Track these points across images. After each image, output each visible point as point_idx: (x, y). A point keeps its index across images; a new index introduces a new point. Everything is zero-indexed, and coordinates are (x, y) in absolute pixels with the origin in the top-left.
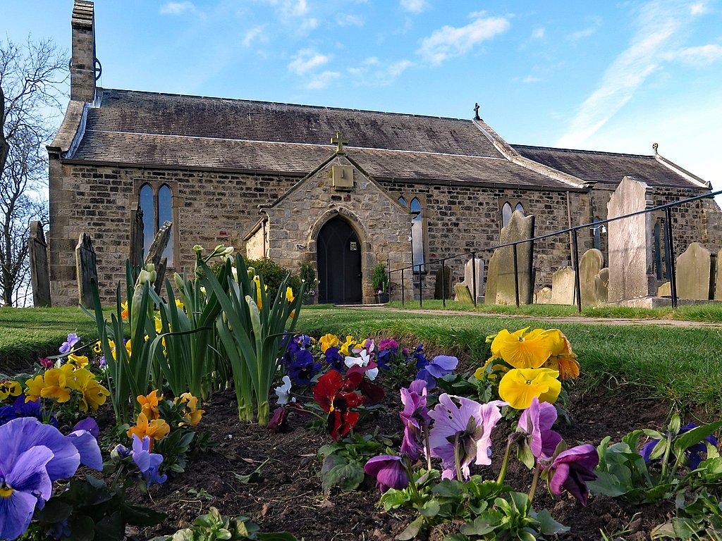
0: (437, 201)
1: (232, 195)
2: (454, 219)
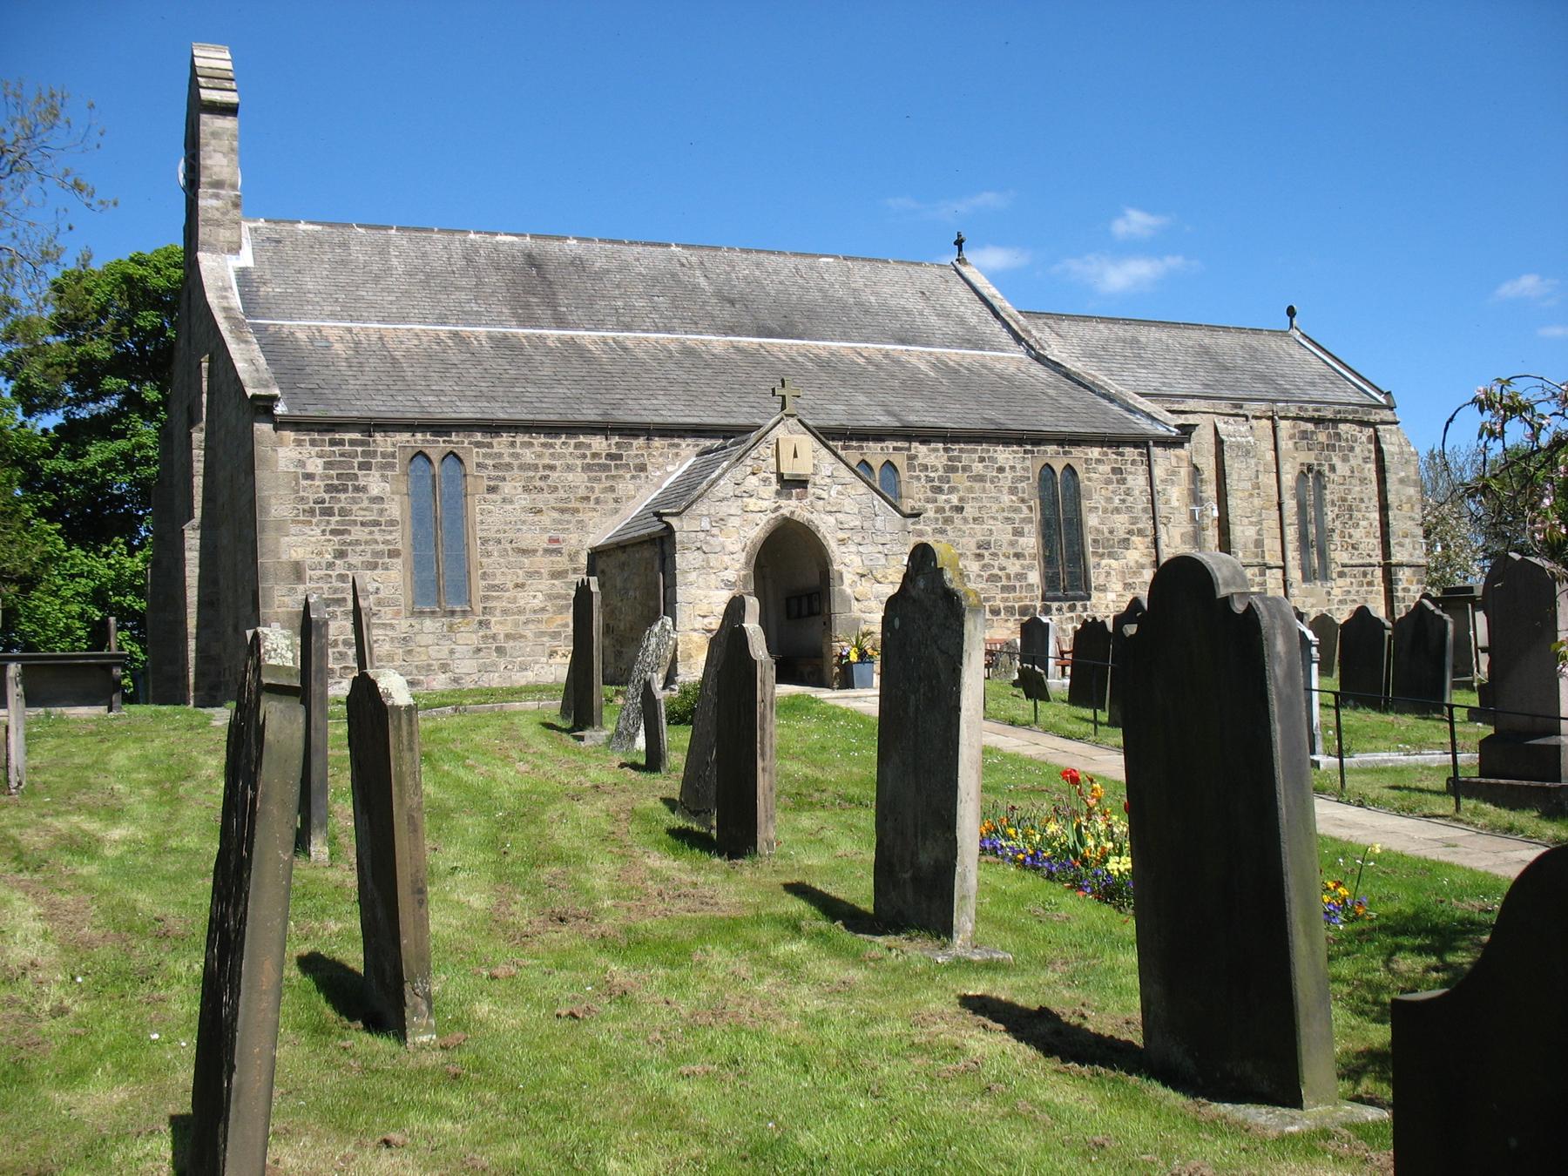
0: (925, 468)
1: (569, 468)
2: (954, 499)
